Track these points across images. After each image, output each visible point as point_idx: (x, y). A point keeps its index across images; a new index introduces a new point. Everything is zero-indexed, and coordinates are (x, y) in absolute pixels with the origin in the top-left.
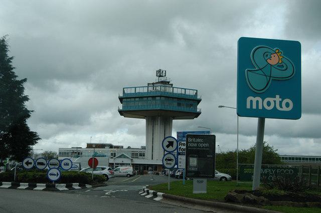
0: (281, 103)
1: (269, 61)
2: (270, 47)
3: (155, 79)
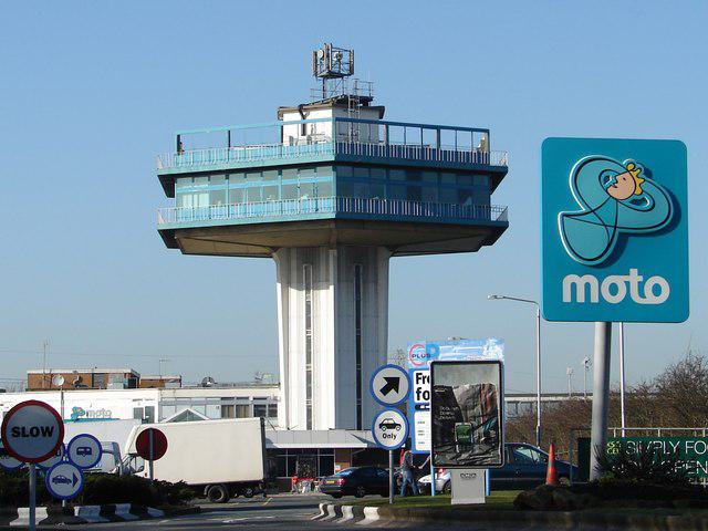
0: (641, 285)
1: (612, 191)
2: (616, 158)
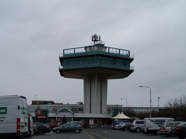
3: (91, 43)
